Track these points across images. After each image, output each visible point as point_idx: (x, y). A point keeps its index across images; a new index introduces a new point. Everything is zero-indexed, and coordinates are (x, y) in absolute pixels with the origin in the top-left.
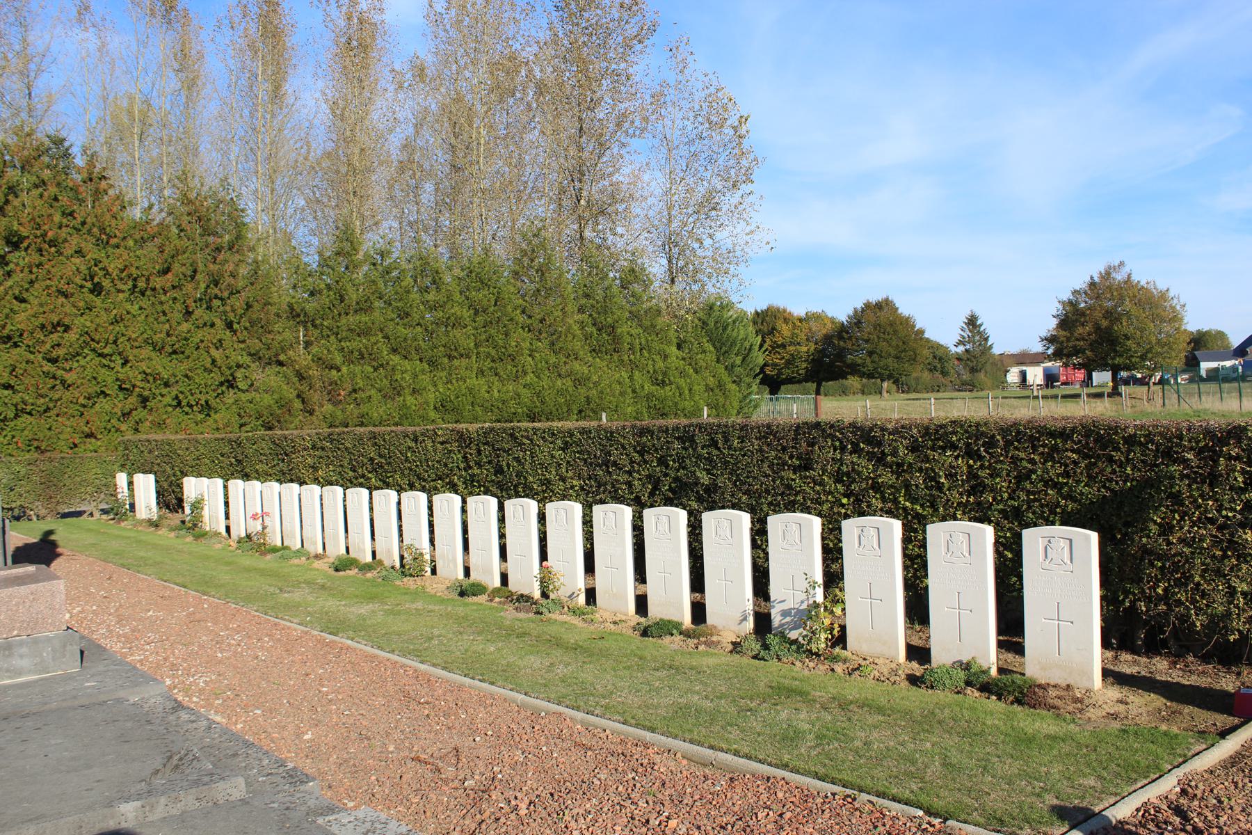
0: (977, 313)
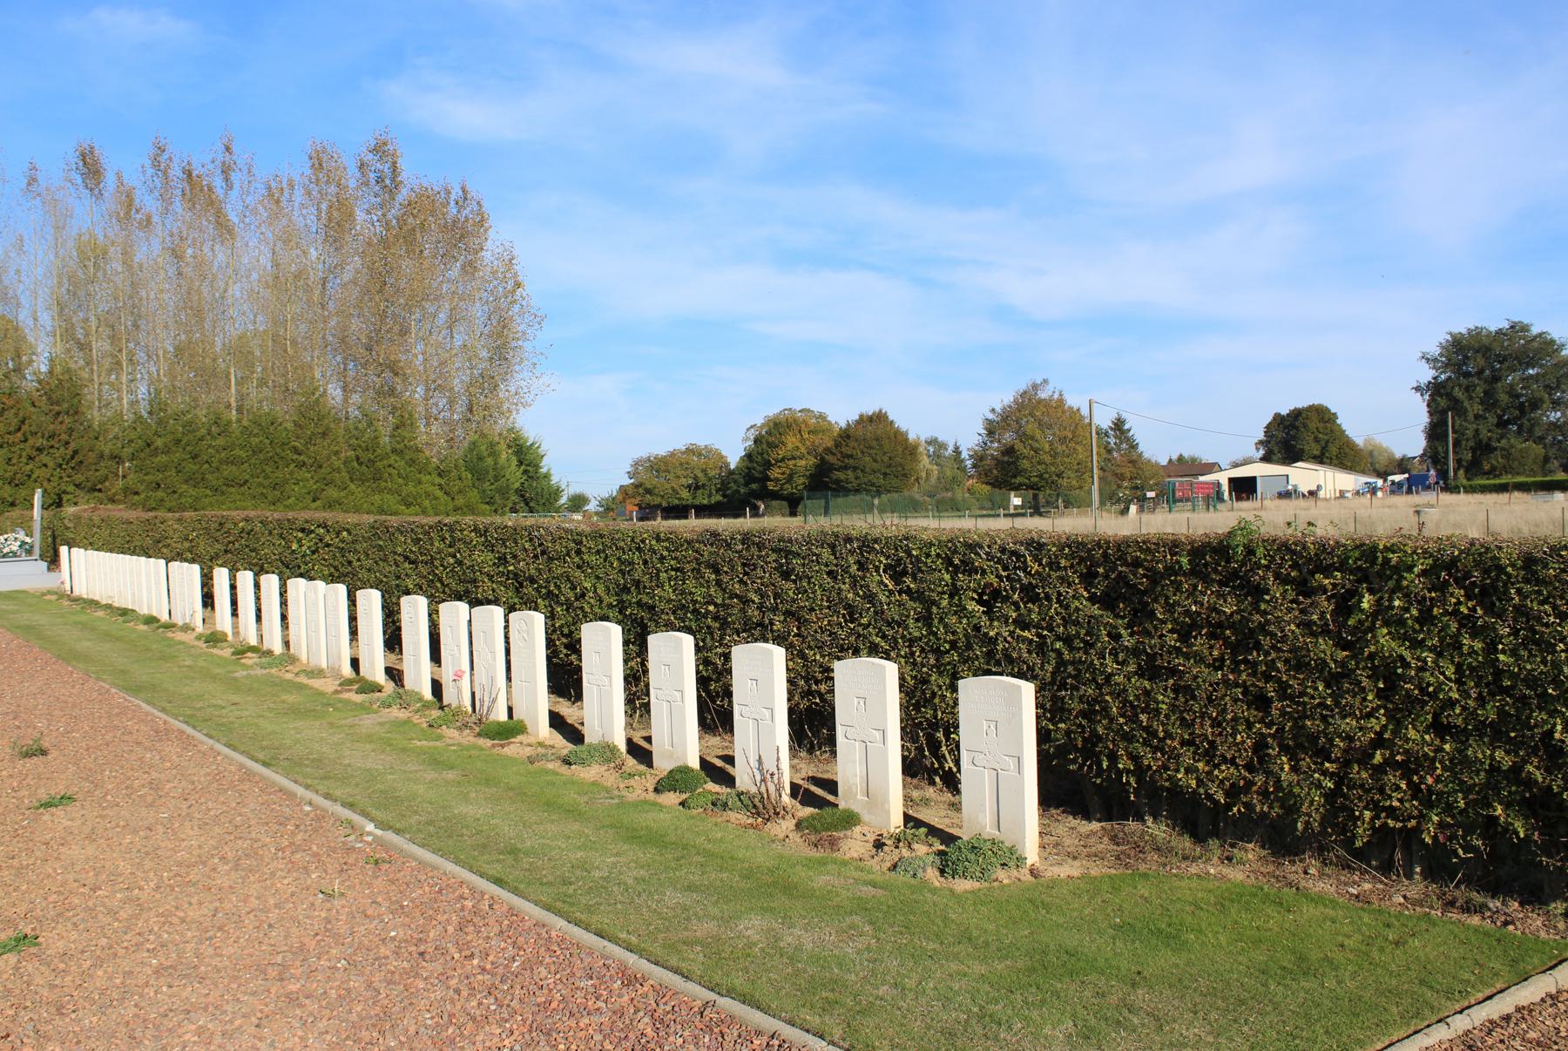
0: (1124, 416)
